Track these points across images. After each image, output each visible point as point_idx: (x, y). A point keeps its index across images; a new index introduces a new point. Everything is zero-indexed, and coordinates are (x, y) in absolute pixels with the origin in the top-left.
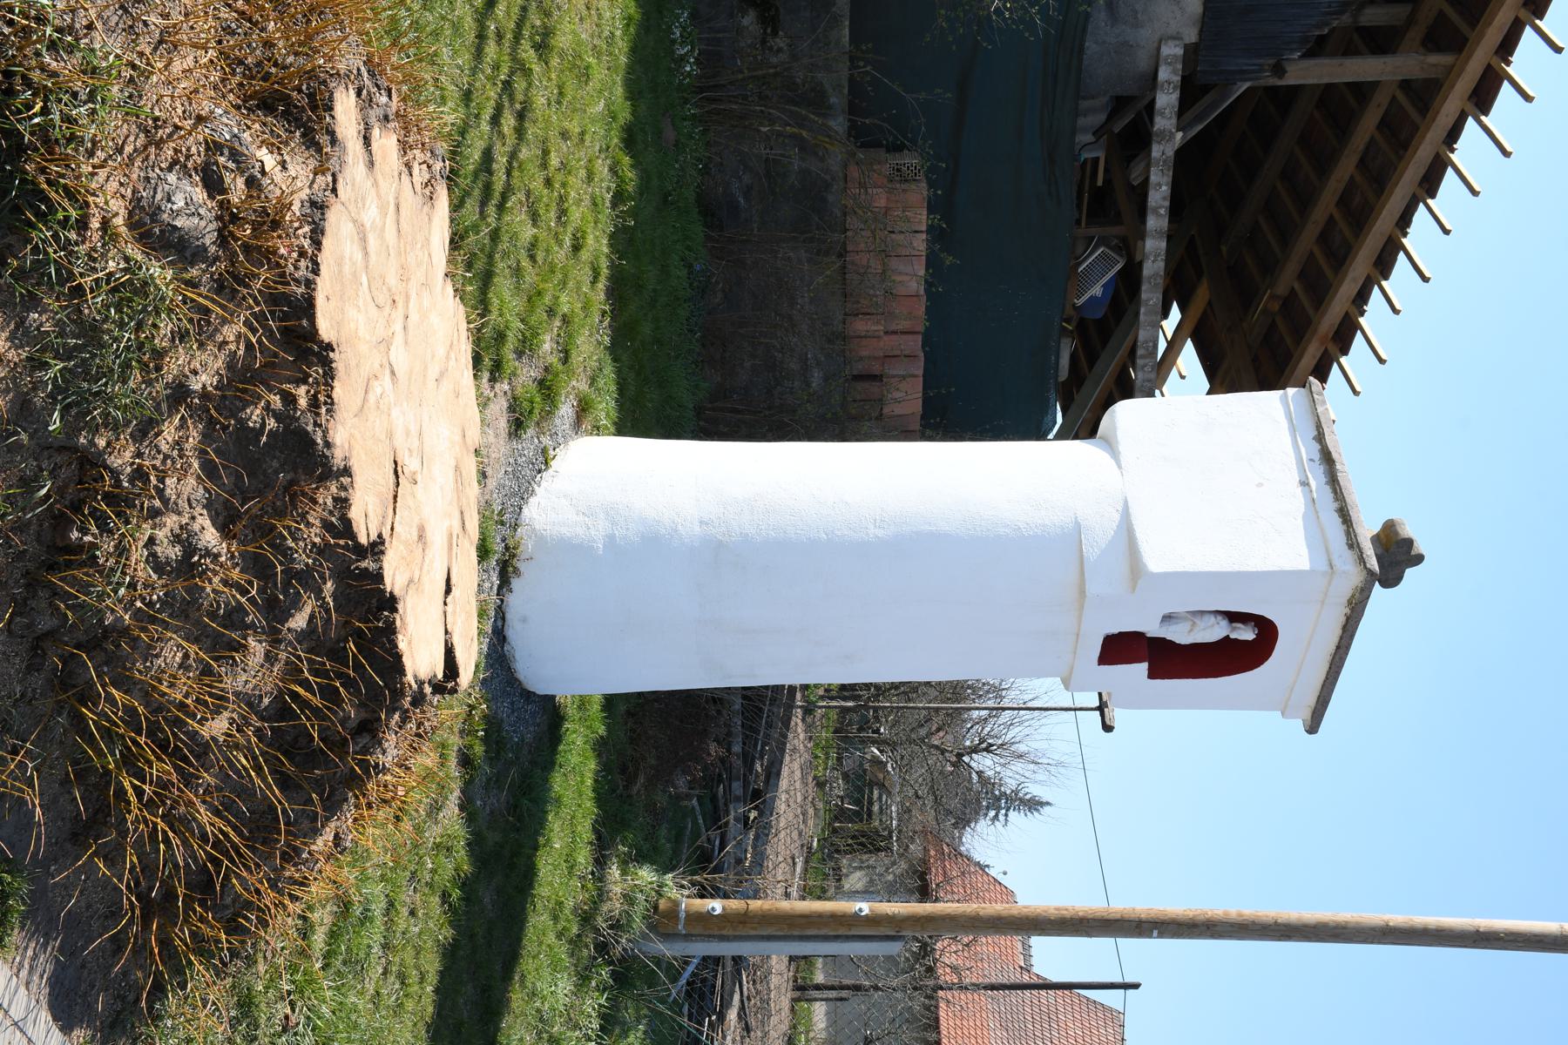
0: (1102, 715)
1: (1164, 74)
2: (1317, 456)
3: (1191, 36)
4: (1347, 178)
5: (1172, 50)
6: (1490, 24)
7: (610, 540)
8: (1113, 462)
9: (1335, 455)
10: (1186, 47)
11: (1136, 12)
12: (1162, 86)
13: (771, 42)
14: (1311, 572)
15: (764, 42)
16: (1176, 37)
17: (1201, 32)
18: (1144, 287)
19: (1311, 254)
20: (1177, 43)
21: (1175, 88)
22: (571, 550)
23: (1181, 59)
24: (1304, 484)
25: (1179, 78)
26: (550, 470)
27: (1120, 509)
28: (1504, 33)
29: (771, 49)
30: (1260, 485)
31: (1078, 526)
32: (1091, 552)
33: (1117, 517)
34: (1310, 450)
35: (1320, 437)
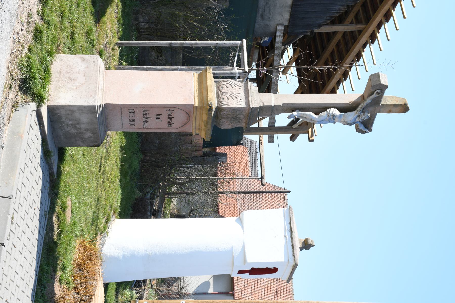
0: (262, 181)
1: (278, 33)
2: (289, 229)
3: (286, 23)
4: (339, 39)
5: (280, 28)
6: (374, 21)
7: (124, 255)
8: (242, 229)
9: (293, 230)
10: (285, 27)
11: (270, 18)
12: (278, 36)
13: (160, 58)
14: (284, 262)
15: (158, 58)
16: (282, 24)
17: (289, 23)
18: (272, 85)
19: (328, 58)
20: (282, 26)
21: (281, 37)
22: (114, 259)
23: (283, 30)
24: (285, 237)
25: (283, 35)
26: (108, 237)
27: (243, 244)
28: (378, 23)
29: (160, 60)
30: (275, 237)
31: (233, 248)
32: (235, 255)
33: (242, 246)
34: (288, 227)
35: (290, 223)
